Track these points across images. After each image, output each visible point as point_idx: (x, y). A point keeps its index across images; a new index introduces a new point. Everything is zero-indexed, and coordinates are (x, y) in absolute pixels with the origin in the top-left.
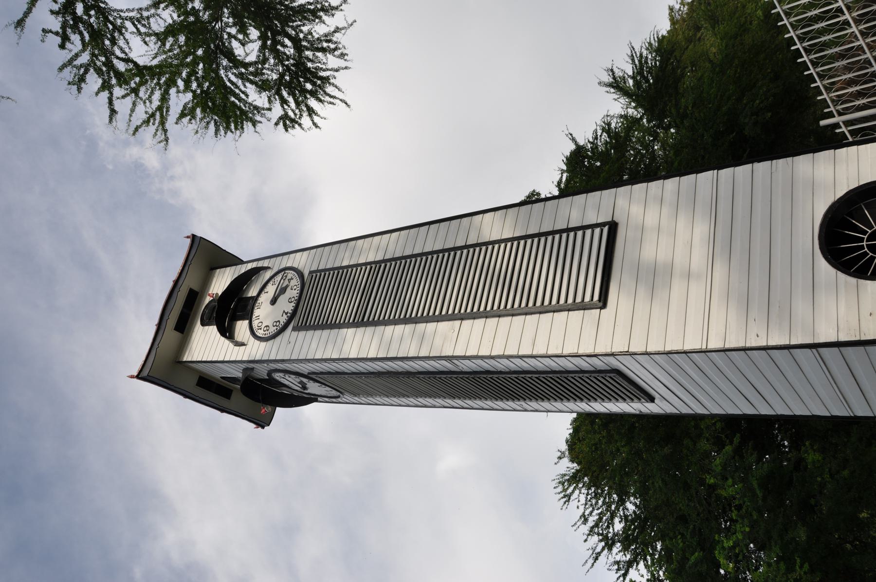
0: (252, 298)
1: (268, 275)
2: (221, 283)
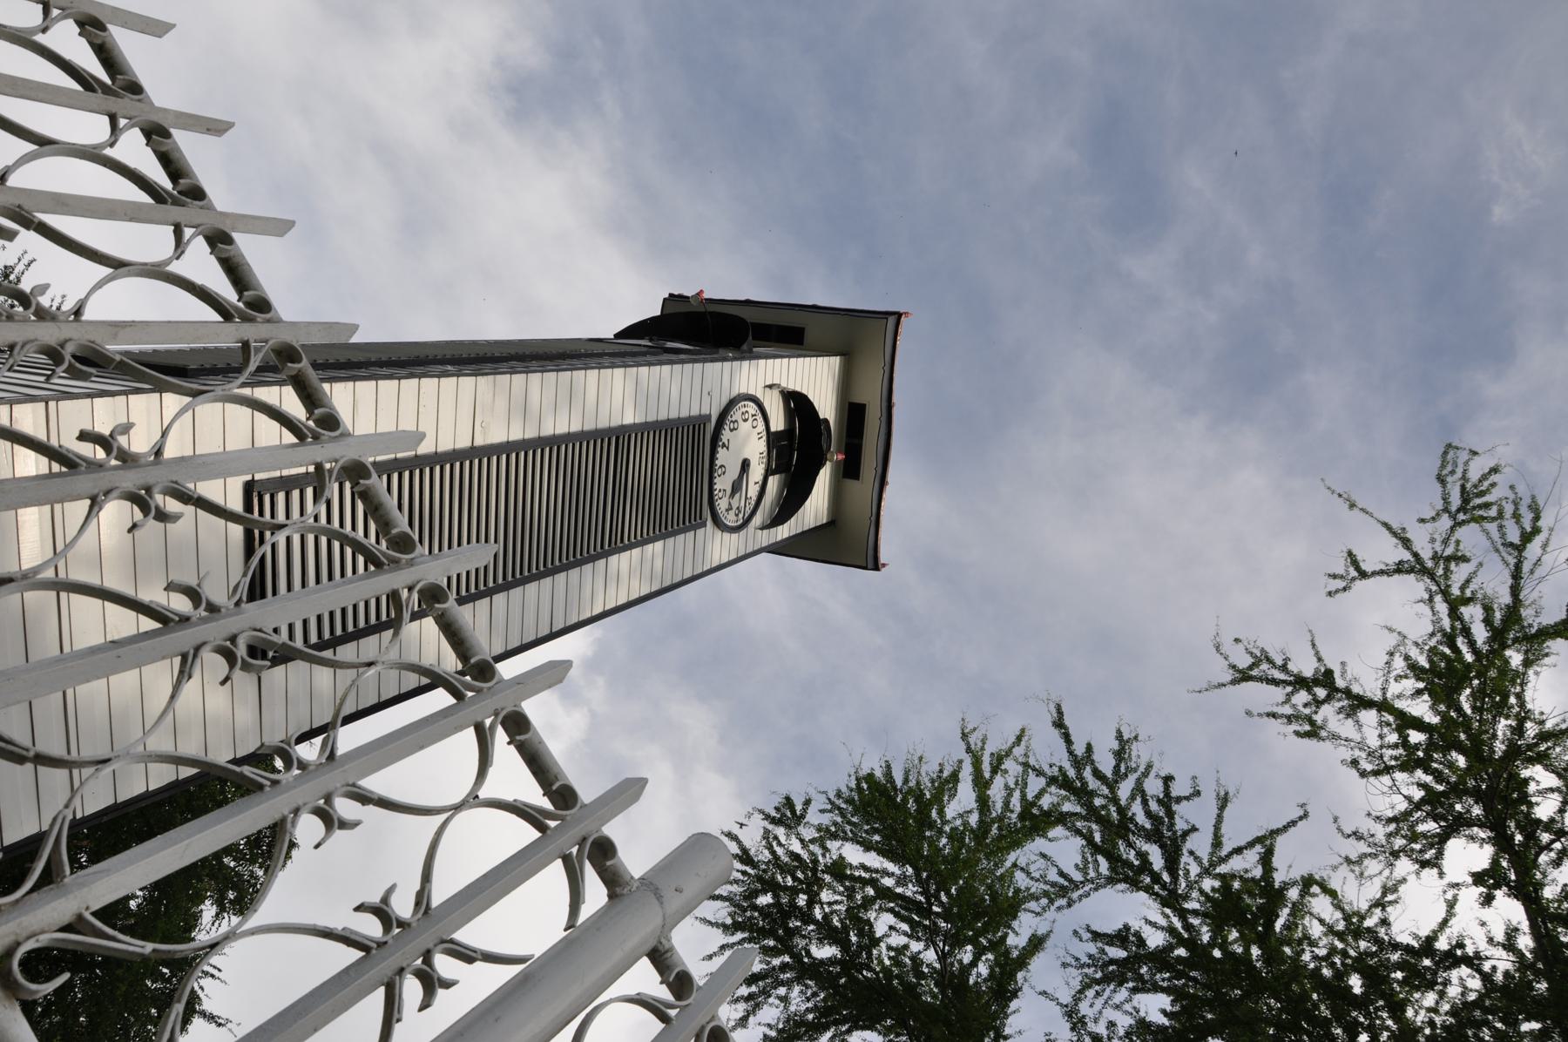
0: (773, 473)
1: (758, 520)
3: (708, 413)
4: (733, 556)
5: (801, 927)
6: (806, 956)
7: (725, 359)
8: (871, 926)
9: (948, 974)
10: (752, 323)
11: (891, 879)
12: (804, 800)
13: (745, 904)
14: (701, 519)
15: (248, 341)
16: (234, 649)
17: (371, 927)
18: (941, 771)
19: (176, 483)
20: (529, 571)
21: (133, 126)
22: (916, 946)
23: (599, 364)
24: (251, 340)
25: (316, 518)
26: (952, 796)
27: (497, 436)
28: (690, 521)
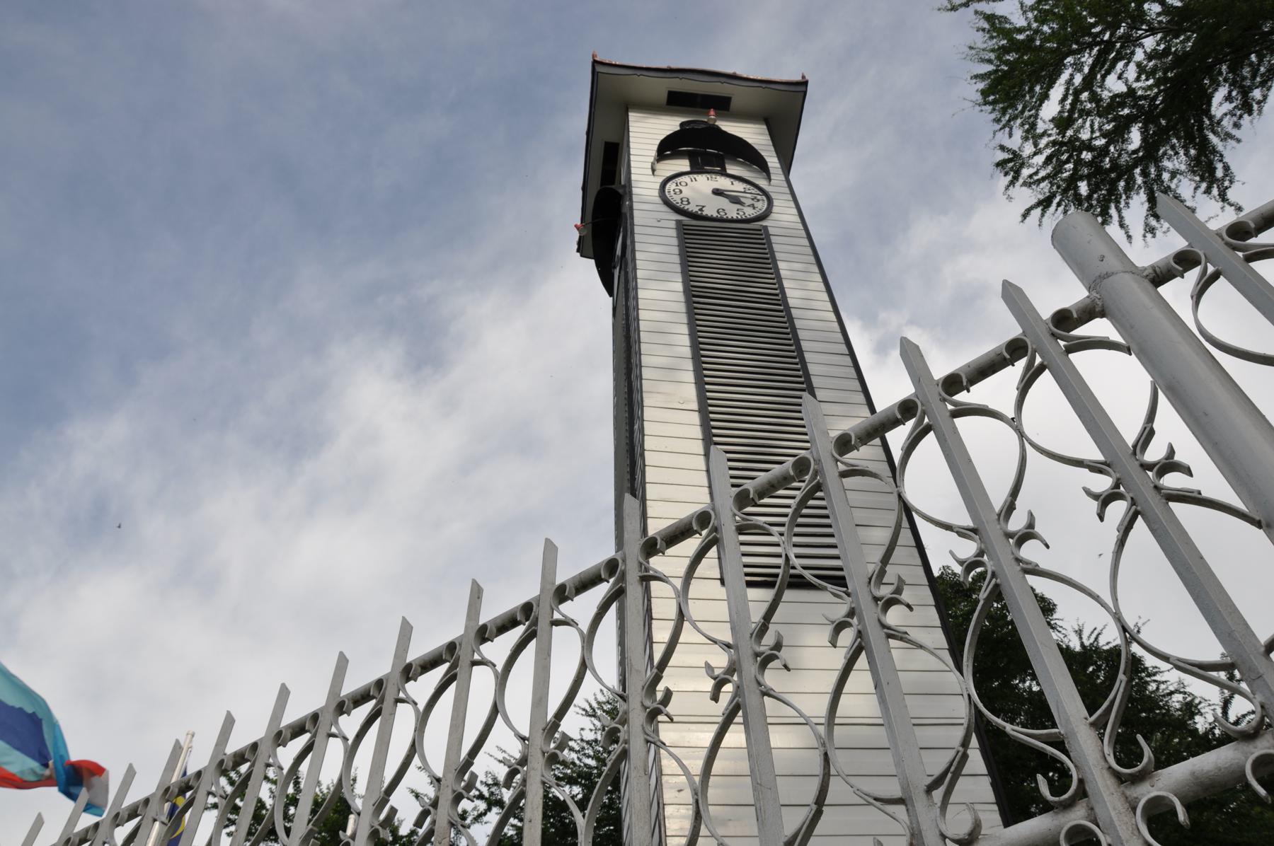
0: (724, 169)
1: (762, 183)
2: (753, 134)
3: (674, 222)
4: (792, 204)
5: (1110, 158)
6: (1137, 154)
7: (631, 208)
8: (1116, 96)
9: (1169, 26)
10: (601, 185)
11: (1075, 77)
12: (1000, 151)
13: (1086, 205)
14: (760, 230)
15: (641, 577)
16: (884, 599)
17: (1118, 510)
18: (983, 30)
19: (752, 634)
20: (799, 370)
21: (479, 650)
22: (1139, 55)
23: (634, 309)
24: (640, 574)
25: (782, 534)
26: (1006, 20)
27: (690, 392)
28: (763, 239)
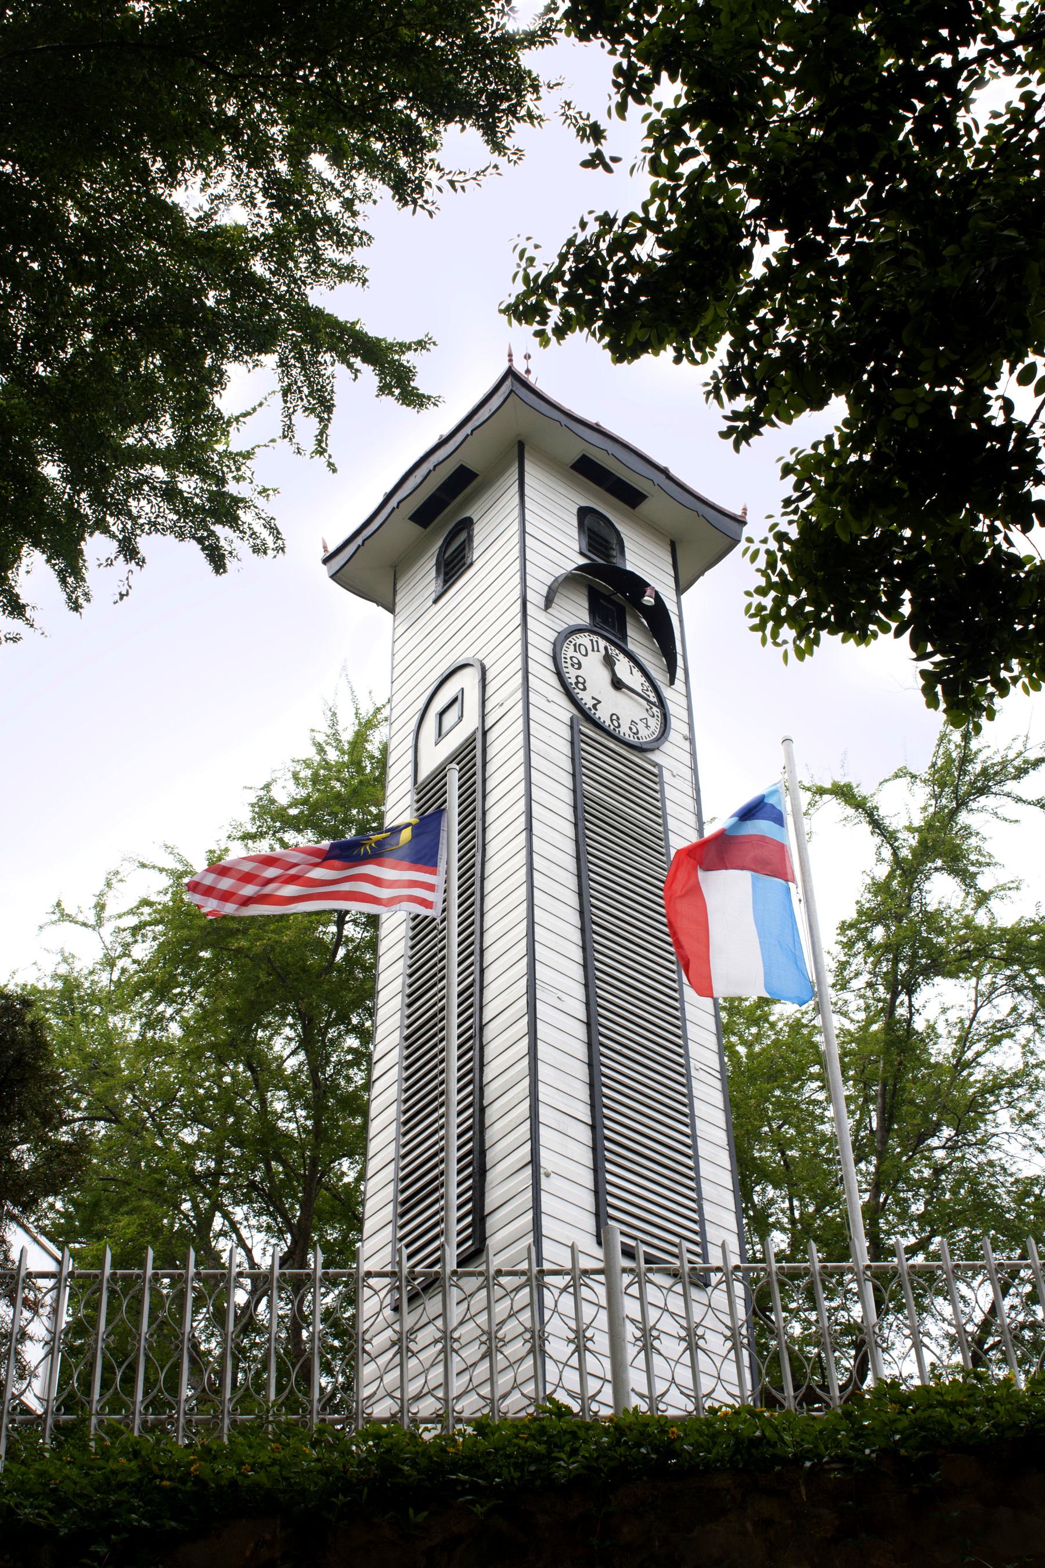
0: (624, 637)
1: (660, 676)
